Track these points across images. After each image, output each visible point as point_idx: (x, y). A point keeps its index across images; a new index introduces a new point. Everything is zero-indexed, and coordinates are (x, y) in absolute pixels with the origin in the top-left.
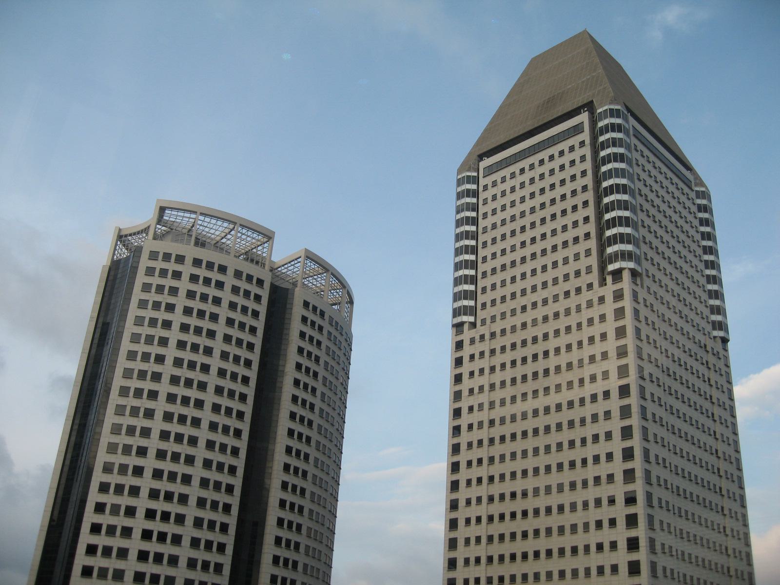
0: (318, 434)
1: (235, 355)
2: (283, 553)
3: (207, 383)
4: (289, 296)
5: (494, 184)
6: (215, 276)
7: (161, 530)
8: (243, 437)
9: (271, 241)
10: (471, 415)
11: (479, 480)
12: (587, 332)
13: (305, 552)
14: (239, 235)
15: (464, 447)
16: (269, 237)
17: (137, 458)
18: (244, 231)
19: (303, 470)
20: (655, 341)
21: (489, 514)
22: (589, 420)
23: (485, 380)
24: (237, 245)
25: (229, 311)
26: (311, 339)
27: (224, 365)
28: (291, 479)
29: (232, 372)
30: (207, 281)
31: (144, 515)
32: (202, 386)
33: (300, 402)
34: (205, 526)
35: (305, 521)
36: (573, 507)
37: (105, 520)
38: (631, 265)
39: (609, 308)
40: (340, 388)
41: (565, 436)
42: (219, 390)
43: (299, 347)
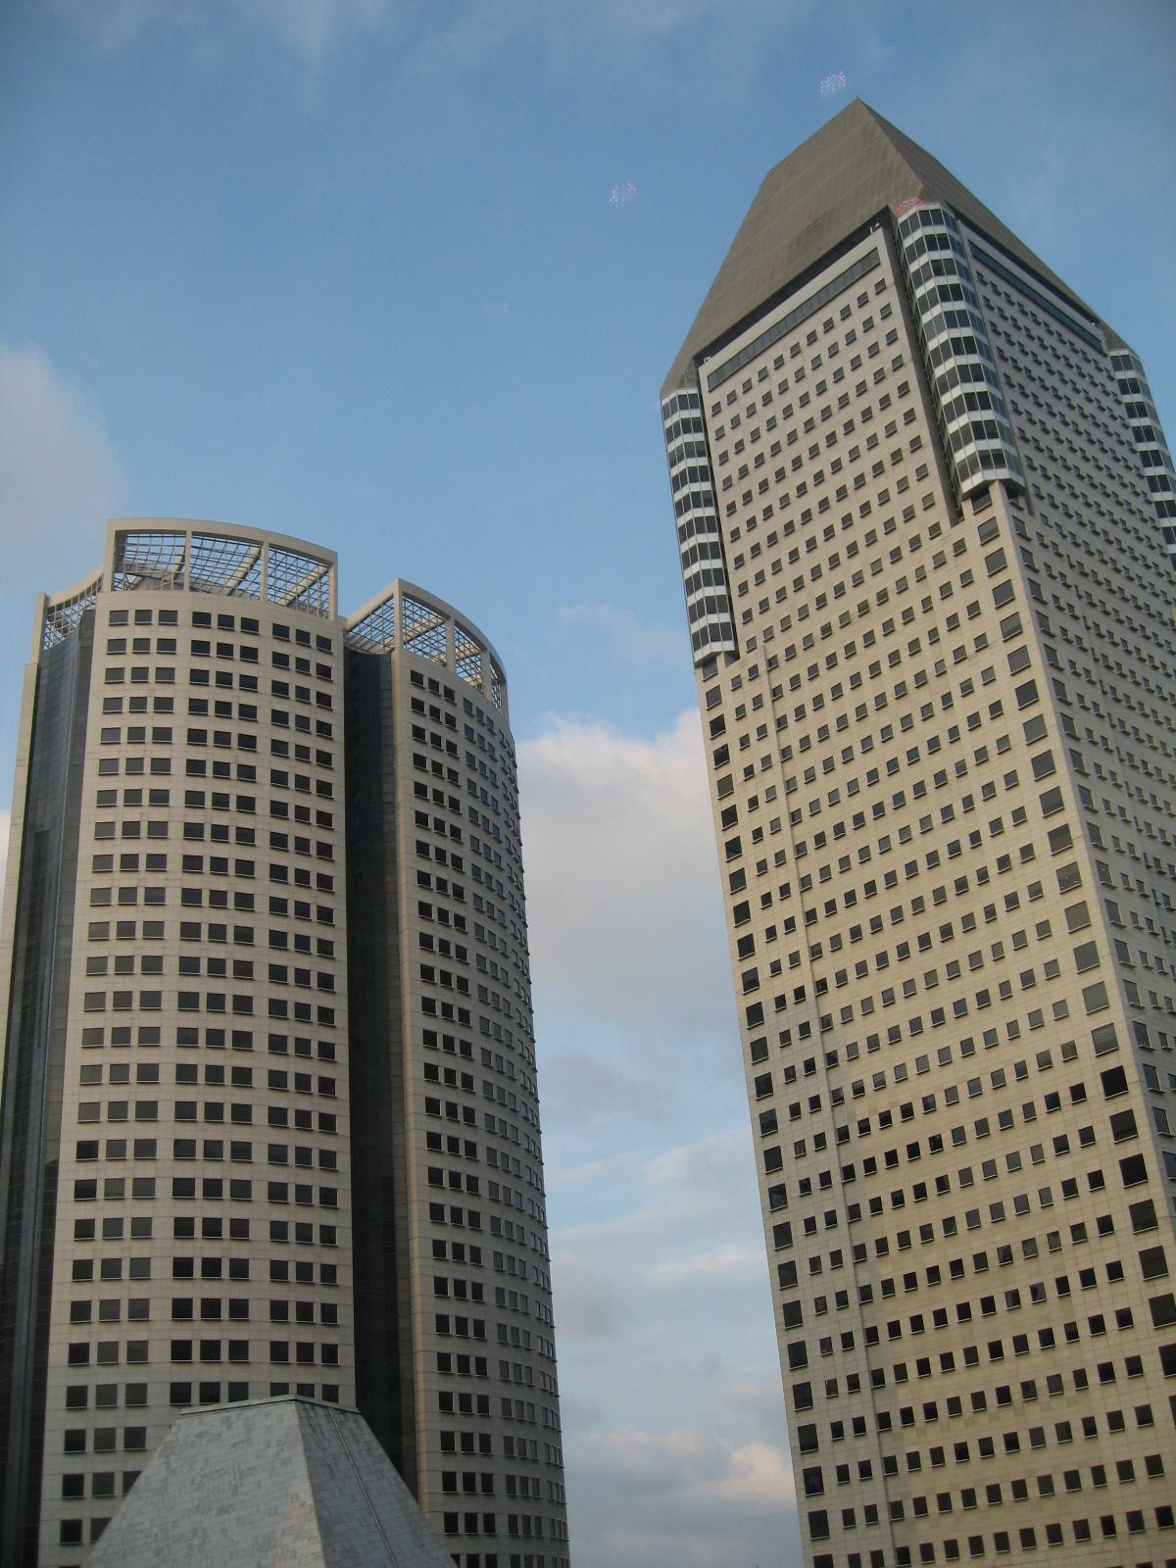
5: (732, 398)
6: (238, 639)
8: (333, 706)
9: (331, 573)
10: (760, 846)
11: (815, 1103)
12: (942, 610)
15: (778, 1080)
19: (470, 1212)
20: (1122, 810)
21: (844, 1165)
22: (1016, 985)
23: (794, 907)
26: (441, 854)
27: (280, 1028)
28: (445, 1128)
30: (219, 866)
33: (441, 1078)
34: (292, 1356)
36: (1014, 1162)
37: (99, 1210)
38: (1004, 473)
39: (976, 558)
41: (947, 874)
42: (278, 906)
43: (415, 755)
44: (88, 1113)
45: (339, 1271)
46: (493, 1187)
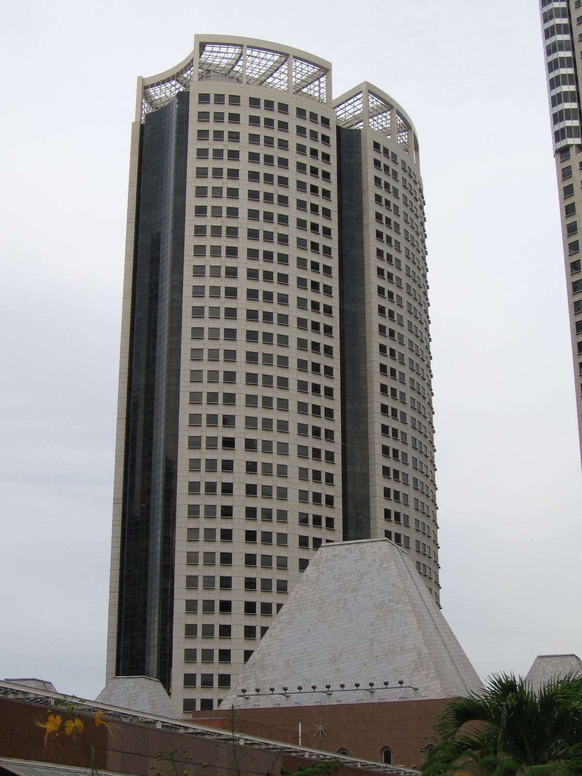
6: (227, 109)
24: (247, 71)
27: (253, 327)
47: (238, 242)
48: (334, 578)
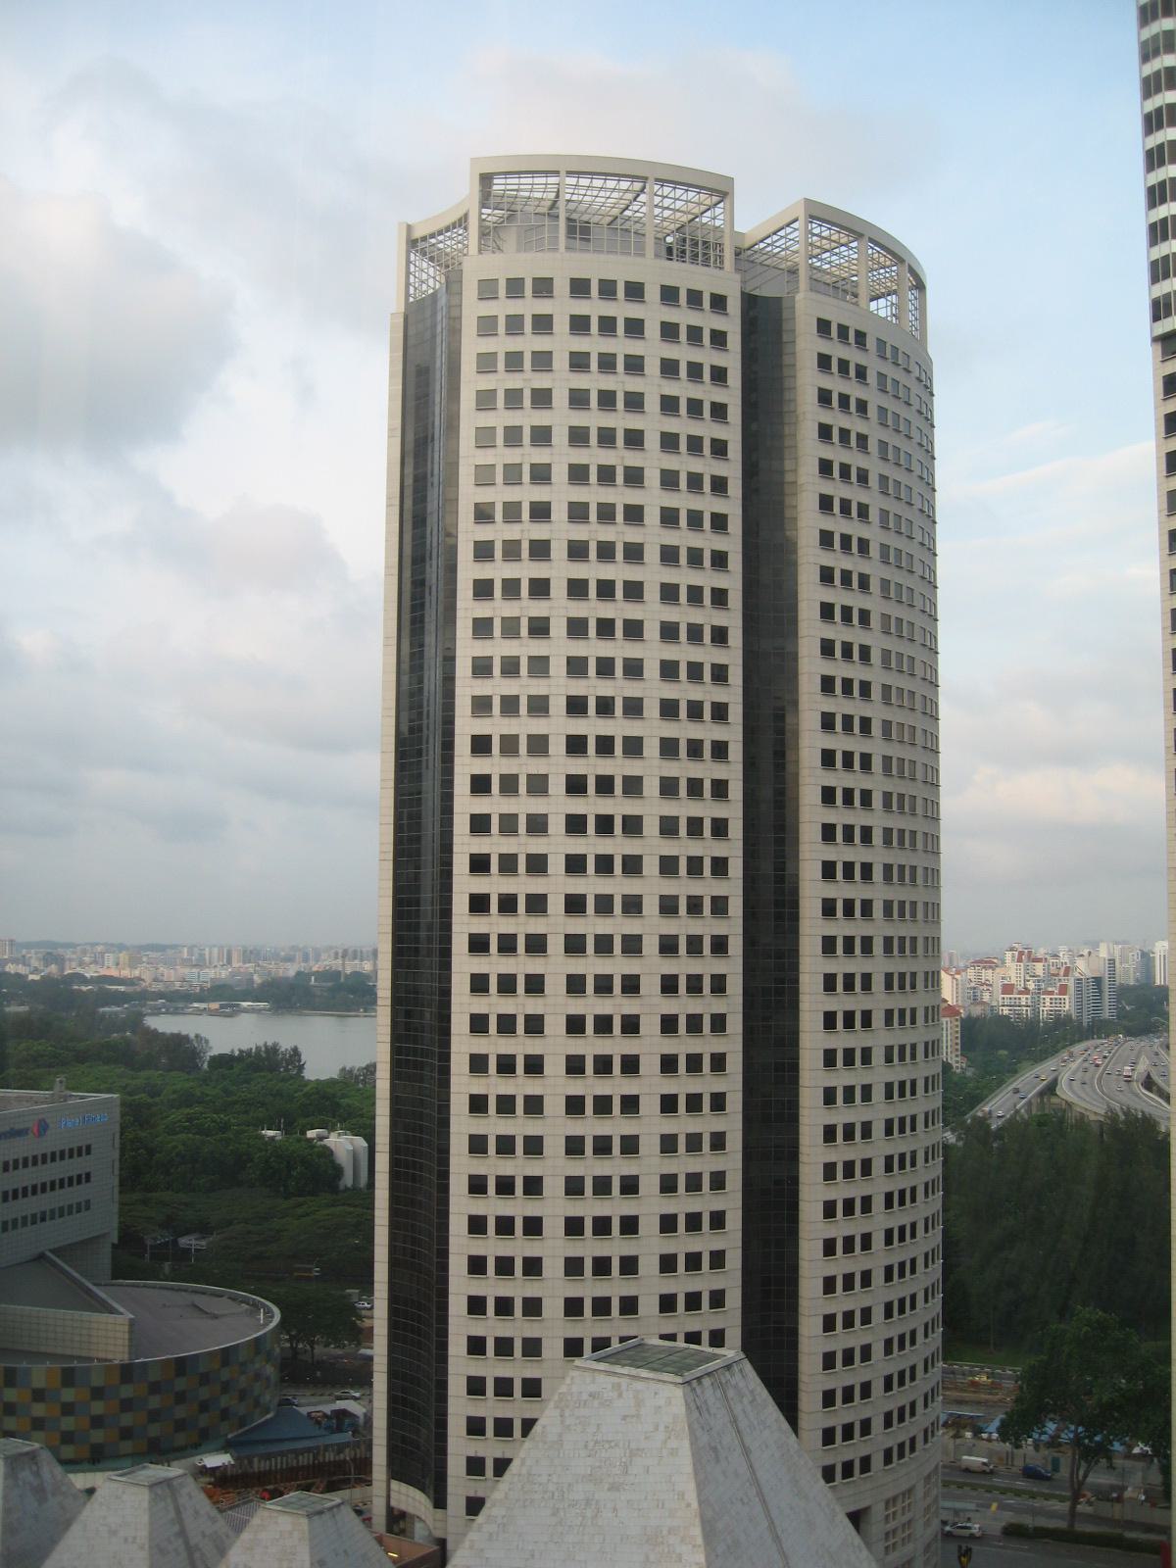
0: (881, 496)
1: (690, 401)
2: (838, 633)
3: (642, 545)
4: (785, 314)
6: (621, 309)
7: (599, 1172)
8: (729, 345)
9: (727, 200)
13: (881, 557)
14: (657, 200)
16: (721, 191)
17: (530, 719)
18: (667, 190)
25: (664, 382)
29: (690, 437)
31: (565, 592)
32: (634, 553)
35: (875, 639)
37: (494, 885)
40: (916, 389)
44: (484, 475)
45: (729, 1019)
46: (884, 514)
47: (551, 568)
48: (586, 1446)
